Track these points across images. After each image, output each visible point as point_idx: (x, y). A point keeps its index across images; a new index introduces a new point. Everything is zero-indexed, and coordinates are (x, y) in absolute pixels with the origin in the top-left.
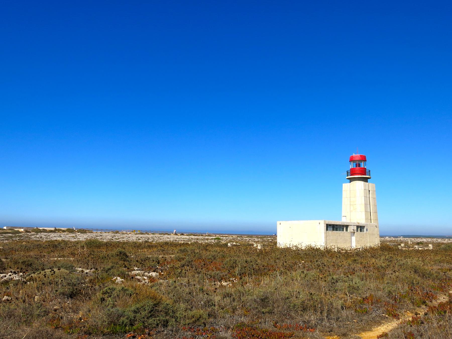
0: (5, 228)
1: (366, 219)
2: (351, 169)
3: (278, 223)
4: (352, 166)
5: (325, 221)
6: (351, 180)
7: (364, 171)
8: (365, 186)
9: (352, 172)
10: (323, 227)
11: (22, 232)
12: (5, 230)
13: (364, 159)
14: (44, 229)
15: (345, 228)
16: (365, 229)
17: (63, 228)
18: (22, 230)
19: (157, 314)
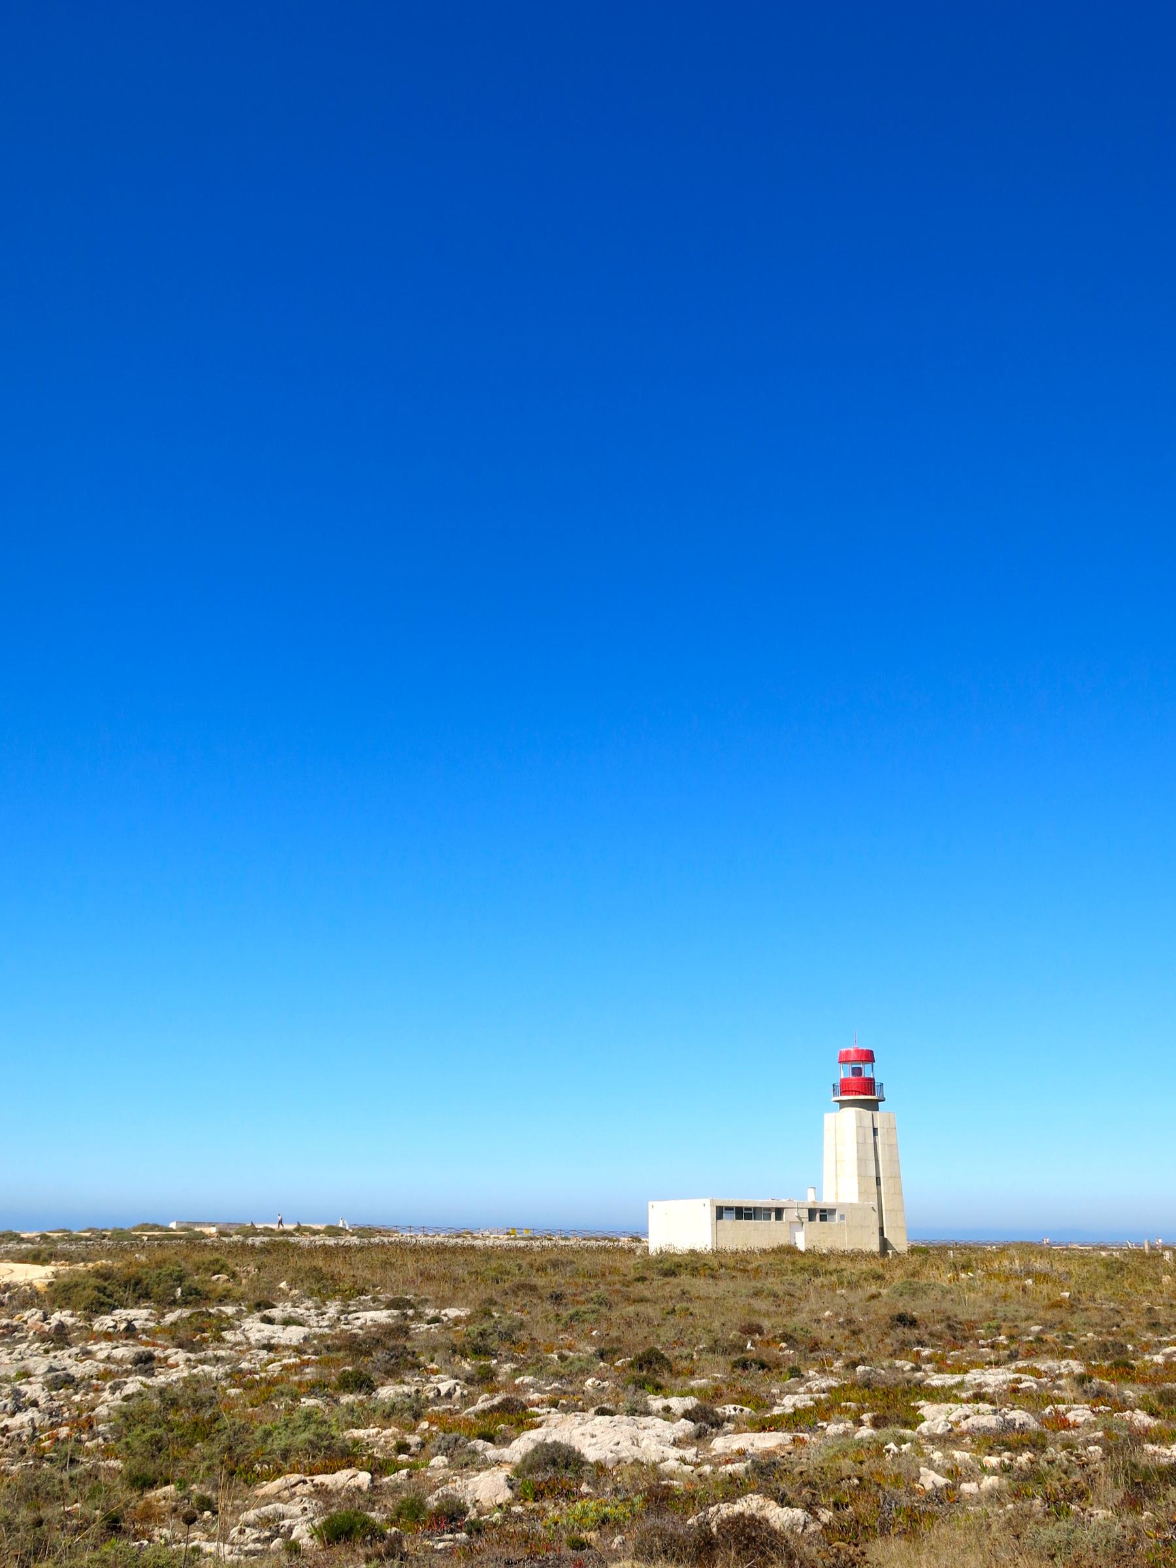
0: (173, 1225)
1: (860, 1193)
2: (843, 1080)
3: (650, 1204)
4: (845, 1072)
5: (712, 1201)
6: (843, 1104)
7: (869, 1086)
8: (860, 1119)
9: (845, 1088)
10: (709, 1214)
11: (210, 1236)
12: (172, 1230)
13: (869, 1057)
14: (266, 1229)
15: (773, 1214)
16: (837, 1216)
17: (318, 1223)
18: (213, 1230)
19: (665, 1378)
